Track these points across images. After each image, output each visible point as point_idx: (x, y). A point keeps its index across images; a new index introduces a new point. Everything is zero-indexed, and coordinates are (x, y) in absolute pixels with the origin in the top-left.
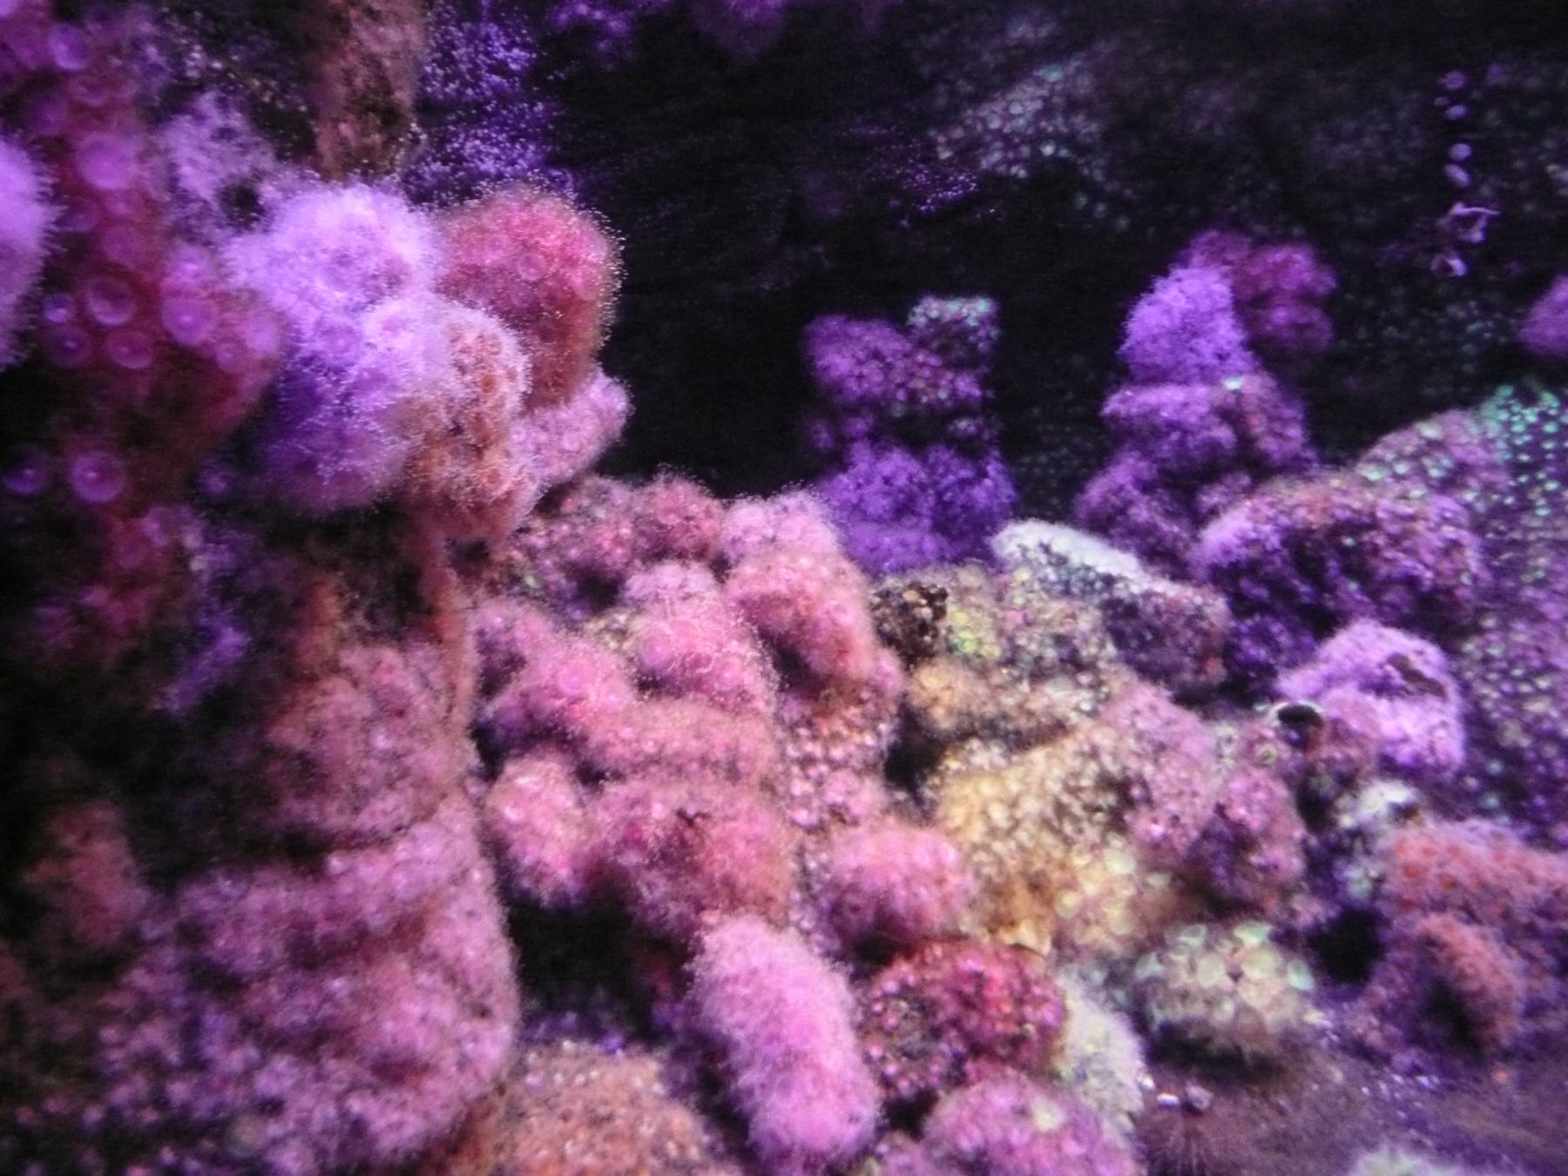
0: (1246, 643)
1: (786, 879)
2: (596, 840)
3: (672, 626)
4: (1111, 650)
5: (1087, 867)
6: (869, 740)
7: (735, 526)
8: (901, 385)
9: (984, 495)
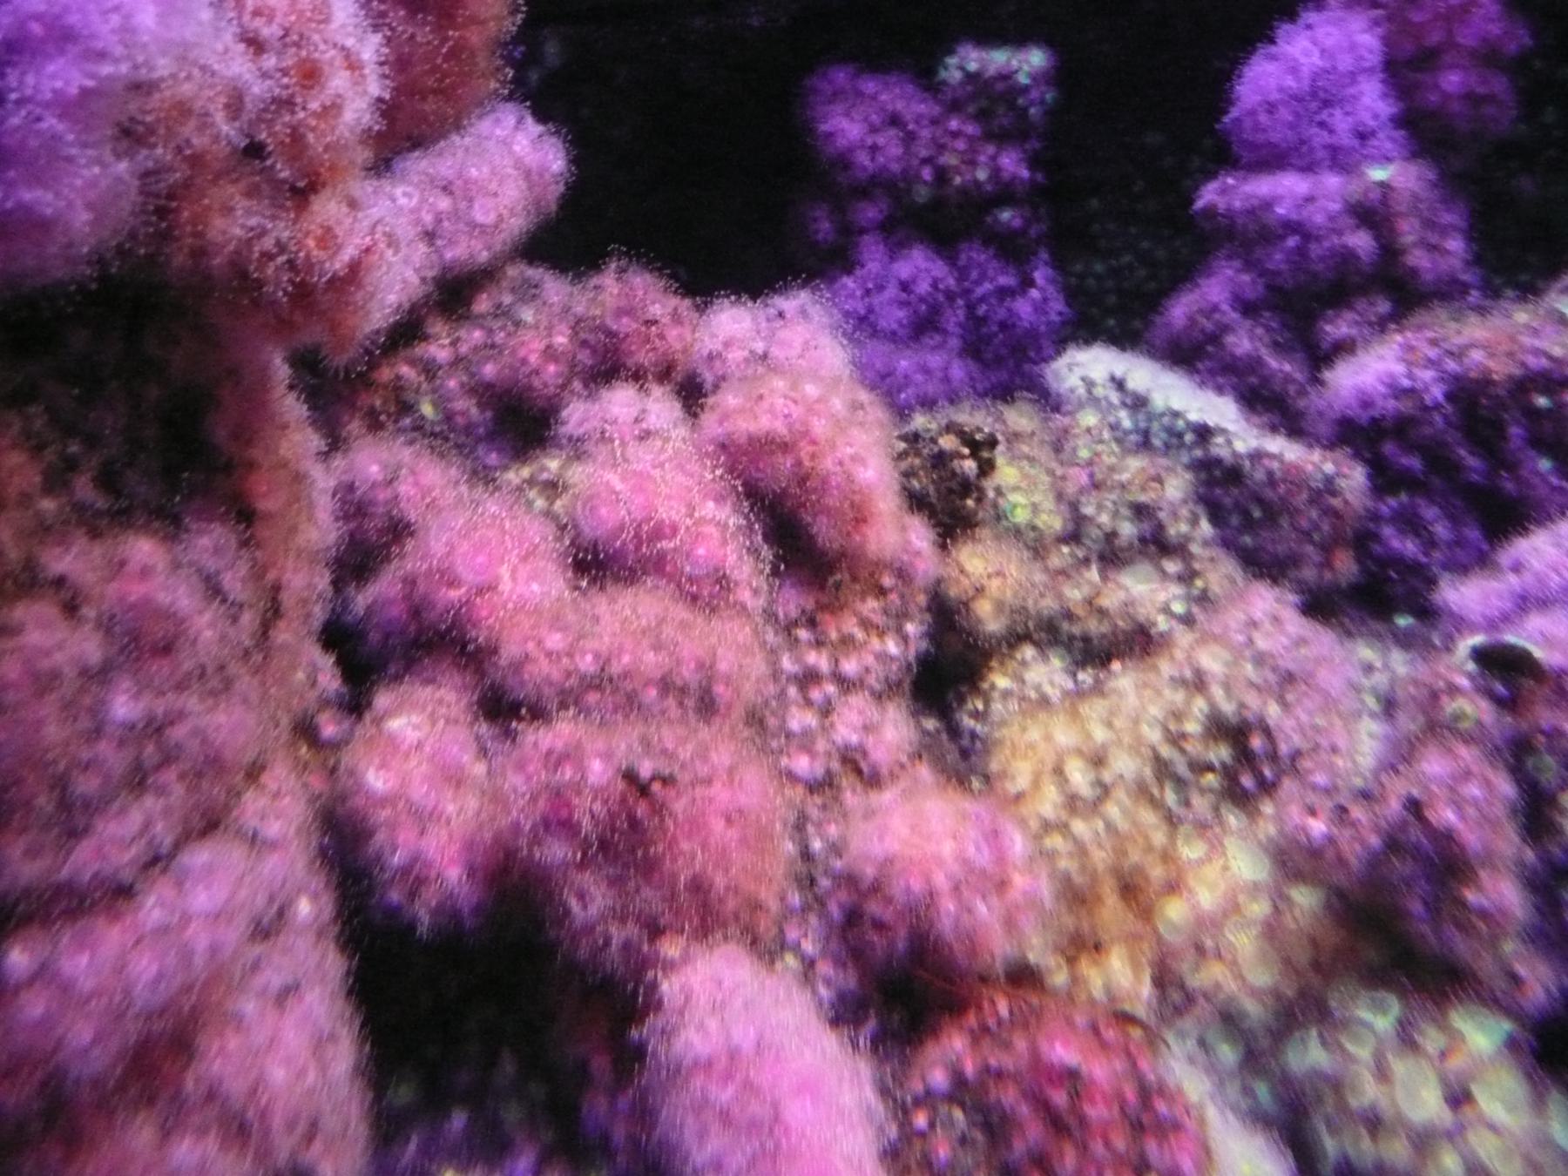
0: (1387, 531)
1: (779, 871)
2: (504, 822)
3: (624, 479)
4: (1206, 528)
5: (1201, 862)
6: (892, 647)
7: (713, 336)
8: (926, 161)
9: (1029, 309)
